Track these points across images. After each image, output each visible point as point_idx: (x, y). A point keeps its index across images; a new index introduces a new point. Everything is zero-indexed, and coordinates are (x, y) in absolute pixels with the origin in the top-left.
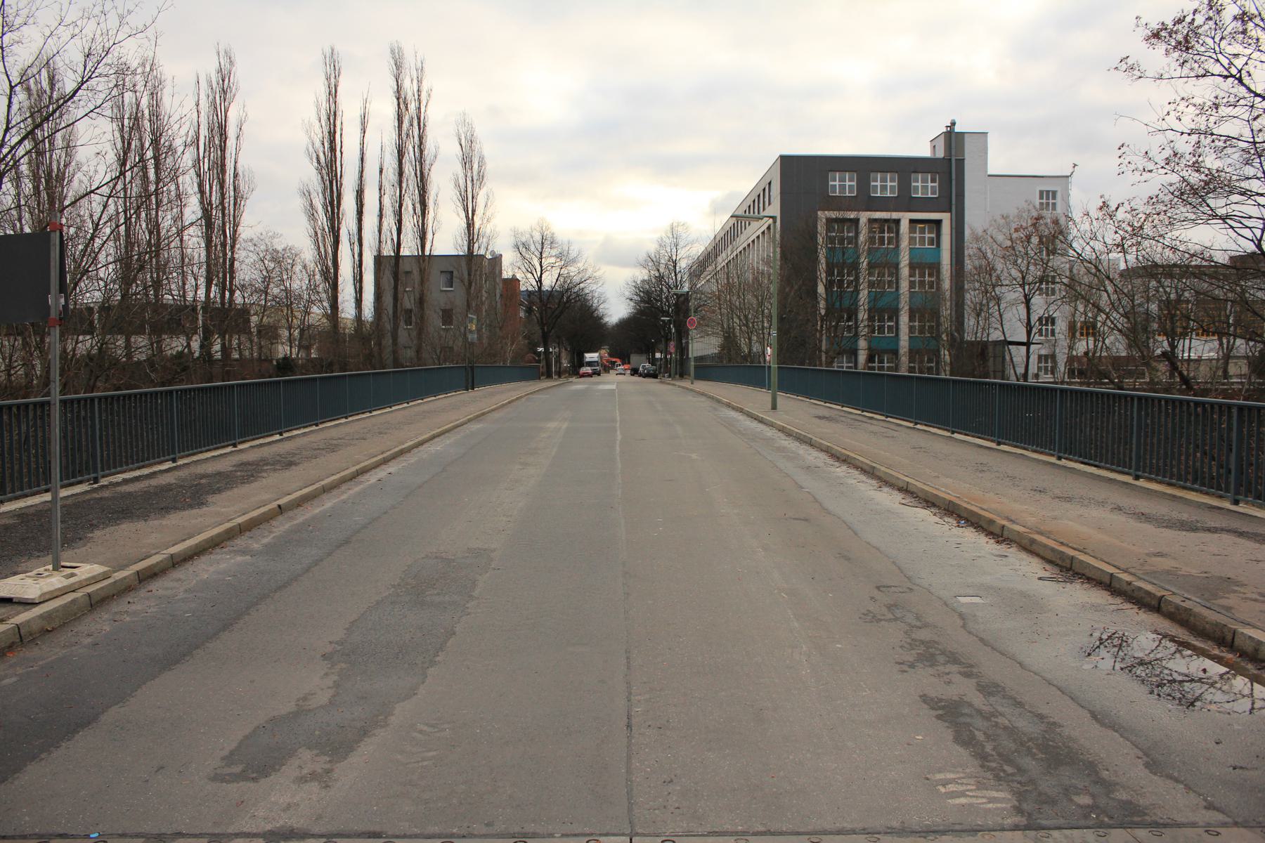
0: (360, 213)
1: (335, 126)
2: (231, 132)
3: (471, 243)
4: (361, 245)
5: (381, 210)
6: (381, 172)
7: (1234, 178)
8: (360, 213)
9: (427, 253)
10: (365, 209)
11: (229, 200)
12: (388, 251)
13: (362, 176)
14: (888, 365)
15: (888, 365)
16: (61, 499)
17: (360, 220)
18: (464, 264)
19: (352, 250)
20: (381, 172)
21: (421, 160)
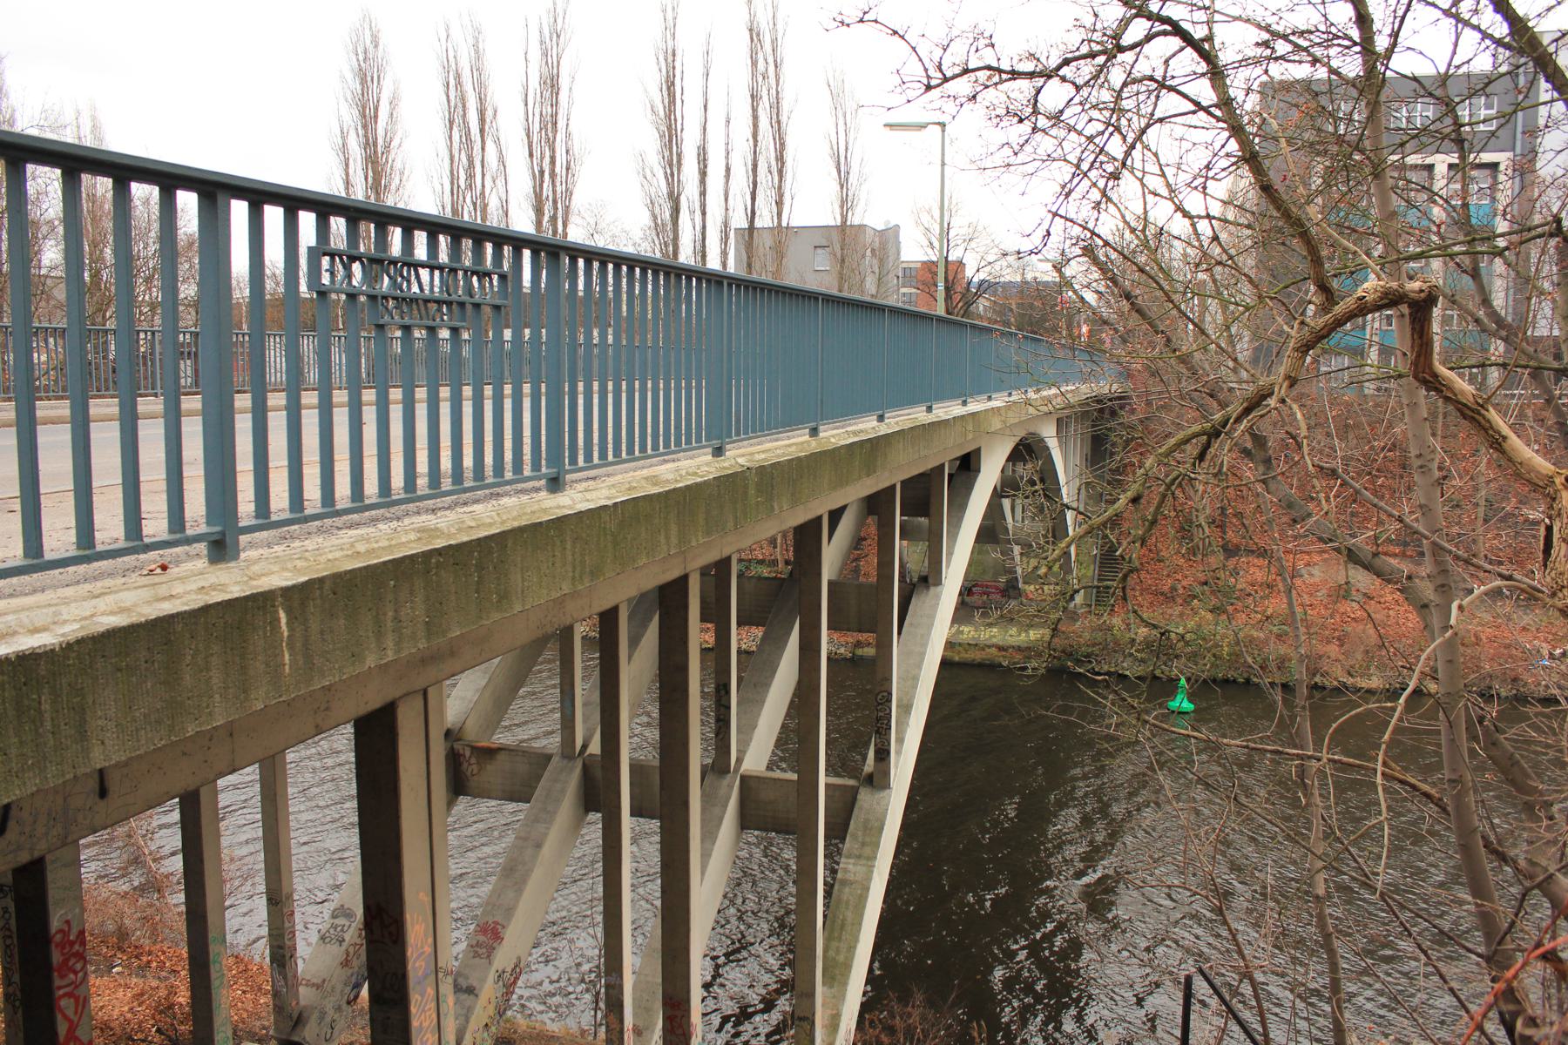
0: (703, 174)
1: (674, 68)
2: (564, 82)
3: (845, 204)
4: (704, 213)
5: (728, 169)
6: (728, 122)
7: (1077, 207)
8: (703, 174)
9: (784, 224)
10: (710, 170)
11: (561, 159)
12: (739, 221)
13: (705, 129)
14: (1324, 751)
15: (1324, 751)
16: (948, 312)
17: (703, 182)
18: (836, 237)
19: (693, 220)
20: (728, 122)
21: (776, 106)
